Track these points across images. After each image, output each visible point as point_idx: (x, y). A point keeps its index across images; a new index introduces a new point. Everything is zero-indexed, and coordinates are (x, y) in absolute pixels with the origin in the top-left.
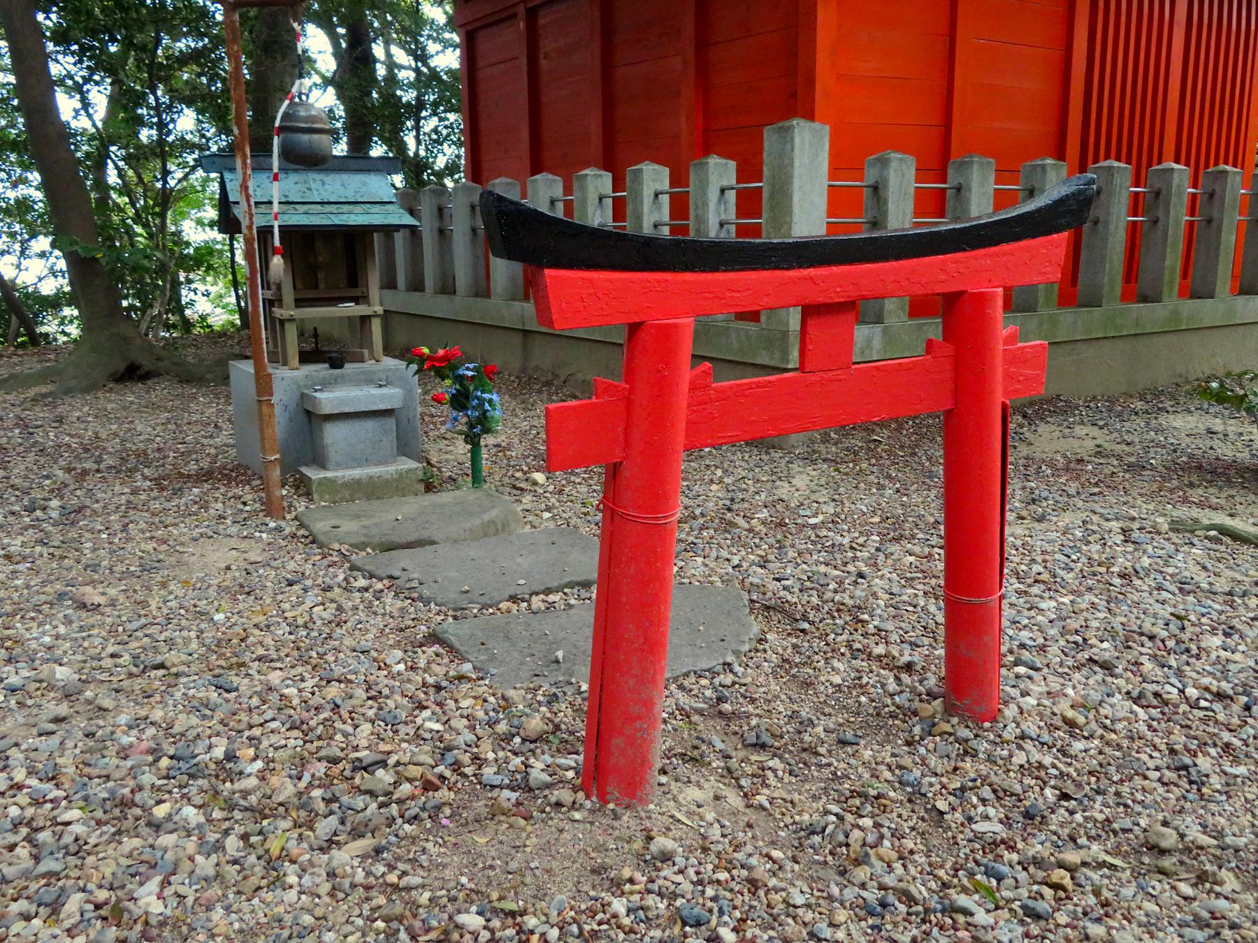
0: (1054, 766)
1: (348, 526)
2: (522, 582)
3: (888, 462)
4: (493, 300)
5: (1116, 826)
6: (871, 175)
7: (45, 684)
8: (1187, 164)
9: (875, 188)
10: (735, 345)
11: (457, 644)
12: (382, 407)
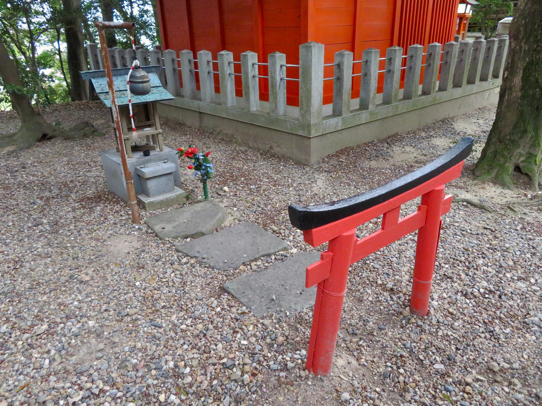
0: (452, 335)
1: (169, 227)
2: (245, 256)
3: (347, 171)
4: (185, 99)
5: (478, 362)
6: (337, 60)
7: (87, 330)
8: (441, 43)
9: (339, 65)
10: (289, 127)
11: (235, 294)
12: (168, 172)
